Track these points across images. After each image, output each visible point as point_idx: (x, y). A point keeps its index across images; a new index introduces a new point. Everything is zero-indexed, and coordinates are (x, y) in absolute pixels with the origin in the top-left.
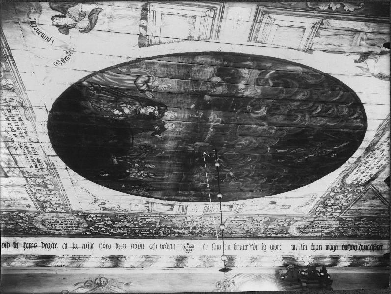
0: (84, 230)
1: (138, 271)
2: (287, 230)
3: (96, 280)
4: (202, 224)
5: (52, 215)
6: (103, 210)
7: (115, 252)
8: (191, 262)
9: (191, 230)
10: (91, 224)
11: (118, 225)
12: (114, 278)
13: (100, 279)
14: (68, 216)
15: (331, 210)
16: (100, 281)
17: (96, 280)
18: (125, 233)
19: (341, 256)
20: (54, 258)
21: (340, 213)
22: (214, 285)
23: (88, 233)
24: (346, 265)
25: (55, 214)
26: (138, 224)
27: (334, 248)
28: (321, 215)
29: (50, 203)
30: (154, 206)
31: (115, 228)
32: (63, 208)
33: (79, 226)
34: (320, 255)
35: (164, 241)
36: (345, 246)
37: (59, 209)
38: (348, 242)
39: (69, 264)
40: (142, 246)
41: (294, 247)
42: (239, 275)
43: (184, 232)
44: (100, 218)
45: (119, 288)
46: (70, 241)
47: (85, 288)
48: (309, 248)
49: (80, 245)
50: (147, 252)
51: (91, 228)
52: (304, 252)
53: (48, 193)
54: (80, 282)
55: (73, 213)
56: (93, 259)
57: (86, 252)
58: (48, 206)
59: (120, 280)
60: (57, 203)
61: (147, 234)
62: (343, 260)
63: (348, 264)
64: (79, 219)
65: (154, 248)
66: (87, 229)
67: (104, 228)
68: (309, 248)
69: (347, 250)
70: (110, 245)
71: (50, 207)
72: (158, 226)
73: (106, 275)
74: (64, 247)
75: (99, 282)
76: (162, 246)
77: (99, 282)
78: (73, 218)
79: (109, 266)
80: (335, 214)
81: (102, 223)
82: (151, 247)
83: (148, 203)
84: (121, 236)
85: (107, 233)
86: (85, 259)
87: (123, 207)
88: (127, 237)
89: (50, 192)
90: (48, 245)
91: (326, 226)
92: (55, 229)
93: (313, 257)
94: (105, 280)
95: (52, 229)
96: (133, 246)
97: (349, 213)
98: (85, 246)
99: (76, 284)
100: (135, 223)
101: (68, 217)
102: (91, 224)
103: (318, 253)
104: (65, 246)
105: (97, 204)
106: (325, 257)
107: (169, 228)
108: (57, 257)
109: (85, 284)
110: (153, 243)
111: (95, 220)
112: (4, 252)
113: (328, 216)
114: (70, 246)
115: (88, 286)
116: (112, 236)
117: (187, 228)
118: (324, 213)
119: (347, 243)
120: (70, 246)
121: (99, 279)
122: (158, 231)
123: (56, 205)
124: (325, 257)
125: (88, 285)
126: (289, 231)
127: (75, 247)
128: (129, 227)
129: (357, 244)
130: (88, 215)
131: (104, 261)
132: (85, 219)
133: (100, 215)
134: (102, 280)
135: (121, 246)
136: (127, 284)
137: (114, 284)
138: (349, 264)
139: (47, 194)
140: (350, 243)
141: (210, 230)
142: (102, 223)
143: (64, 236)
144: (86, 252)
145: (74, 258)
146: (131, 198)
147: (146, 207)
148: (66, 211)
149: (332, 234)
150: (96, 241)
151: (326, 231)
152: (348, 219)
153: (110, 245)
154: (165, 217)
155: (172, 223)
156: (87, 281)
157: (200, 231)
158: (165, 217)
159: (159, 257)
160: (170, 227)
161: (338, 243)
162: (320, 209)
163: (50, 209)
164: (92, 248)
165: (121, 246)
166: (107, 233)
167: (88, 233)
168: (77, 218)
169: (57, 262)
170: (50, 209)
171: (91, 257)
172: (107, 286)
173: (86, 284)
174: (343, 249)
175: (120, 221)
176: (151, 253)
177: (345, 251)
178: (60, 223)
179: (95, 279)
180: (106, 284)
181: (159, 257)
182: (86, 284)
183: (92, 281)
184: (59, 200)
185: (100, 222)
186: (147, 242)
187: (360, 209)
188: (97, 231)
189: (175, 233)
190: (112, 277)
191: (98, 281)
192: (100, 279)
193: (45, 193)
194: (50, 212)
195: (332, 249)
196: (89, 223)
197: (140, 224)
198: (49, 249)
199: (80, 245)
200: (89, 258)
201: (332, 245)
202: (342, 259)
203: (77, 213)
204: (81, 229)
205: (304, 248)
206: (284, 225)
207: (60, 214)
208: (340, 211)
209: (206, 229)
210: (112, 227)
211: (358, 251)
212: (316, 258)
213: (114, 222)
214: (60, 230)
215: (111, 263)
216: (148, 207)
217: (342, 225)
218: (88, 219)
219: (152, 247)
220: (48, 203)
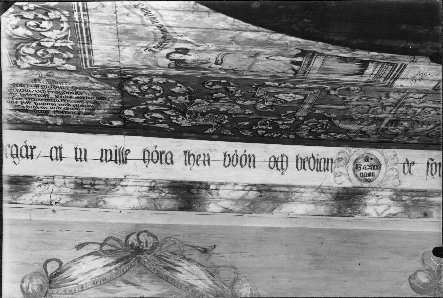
0: (108, 116)
1: (235, 221)
3: (128, 237)
4: (419, 111)
5: (35, 74)
6: (177, 67)
7: (181, 172)
8: (376, 207)
9: (383, 126)
10: (128, 100)
11: (202, 105)
12: (173, 233)
13: (138, 236)
14: (79, 81)
16: (139, 242)
17: (128, 237)
18: (210, 126)
20: (29, 183)
23: (116, 123)
25: (44, 73)
26: (254, 106)
29: (39, 45)
30: (317, 63)
31: (190, 113)
32: (68, 59)
33: (97, 104)
35: (306, 150)
37: (58, 61)
39: (68, 199)
40: (250, 161)
43: (364, 129)
44: (159, 89)
45: (184, 258)
46: (69, 141)
47: (101, 257)
49: (94, 154)
50: (262, 175)
51: (127, 112)
53: (40, 16)
54: (89, 240)
55: (90, 72)
56: (129, 190)
57: (110, 171)
58: (32, 51)
59: (186, 240)
60: (58, 44)
61: (267, 131)
64: (104, 89)
65: (279, 167)
66: (117, 113)
67: (161, 112)
70: (169, 156)
71: (35, 55)
72: (301, 114)
73: (152, 226)
75: (136, 243)
76: (302, 163)
77: (136, 243)
78: (87, 85)
79: (169, 207)
81: (160, 100)
82: (272, 164)
83: (303, 53)
84: (198, 133)
85: (166, 125)
86: (108, 188)
87: (230, 61)
88: (213, 137)
89: (46, 15)
90: (14, 149)
92: (35, 112)
94: (151, 240)
95: (26, 111)
96: (230, 160)
98: (105, 156)
99: (80, 246)
100: (248, 103)
101: (77, 82)
102: (128, 100)
104: (57, 154)
105: (165, 52)
107: (330, 119)
108: (38, 180)
109: (102, 245)
110: (277, 155)
111: (143, 93)
112: (10, 168)
114: (68, 152)
115: (111, 251)
116: (178, 133)
117: (376, 121)
120: (68, 152)
121: (134, 237)
122: (297, 126)
123: (51, 51)
125: (110, 248)
127: (81, 156)
128: (226, 113)
130: (130, 79)
131: (155, 195)
132: (120, 88)
133: (161, 81)
134: (142, 238)
135: (196, 159)
136: (205, 251)
137: (174, 249)
139: (36, 18)
141: (432, 126)
142: (160, 100)
143: (55, 128)
144: (110, 171)
145: (80, 184)
146: (264, 38)
147: (293, 62)
148: (73, 67)
150: (136, 144)
153: (169, 156)
154: (333, 93)
155: (343, 107)
156: (106, 240)
157: (406, 129)
158: (333, 93)
159: (294, 189)
160: (334, 115)
163: (33, 61)
164: (125, 161)
165: (196, 160)
166: (166, 125)
167: (116, 123)
168: (98, 86)
169: (40, 194)
170: (33, 61)
171: (123, 183)
172: (157, 252)
173: (105, 248)
175: (208, 96)
176: (274, 178)
178: (52, 96)
179: (125, 236)
180: (153, 248)
181: (294, 189)
182: (105, 248)
183: (118, 240)
184: (65, 37)
185: (156, 98)
186: (262, 151)
188: (142, 120)
189: (339, 130)
190: (167, 232)
191: (132, 240)
192: (138, 236)
193: (31, 16)
194: (33, 67)
196: (126, 99)
197: (260, 106)
198: (16, 160)
199: (94, 154)
200: (118, 187)
203: (104, 71)
204: (100, 114)
207: (57, 74)
209: (423, 123)
210: (182, 110)
213: (191, 98)
214: (46, 113)
215: (174, 202)
216: (299, 63)
218: (127, 89)
219: (276, 164)
220: (34, 44)
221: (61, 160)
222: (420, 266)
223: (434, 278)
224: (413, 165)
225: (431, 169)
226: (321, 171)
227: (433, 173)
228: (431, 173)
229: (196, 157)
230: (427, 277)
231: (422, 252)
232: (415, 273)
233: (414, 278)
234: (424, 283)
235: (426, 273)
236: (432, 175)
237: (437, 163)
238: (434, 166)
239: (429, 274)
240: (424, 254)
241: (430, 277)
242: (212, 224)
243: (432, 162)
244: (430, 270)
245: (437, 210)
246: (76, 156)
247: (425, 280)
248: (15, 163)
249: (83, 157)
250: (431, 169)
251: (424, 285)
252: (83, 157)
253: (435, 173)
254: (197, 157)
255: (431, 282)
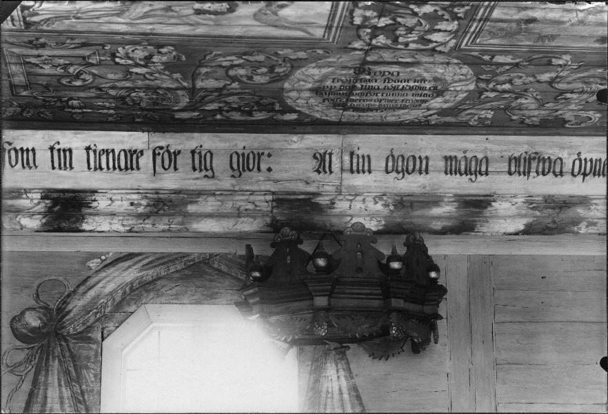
2: (279, 95)
15: (415, 21)
19: (503, 197)
21: (455, 34)
22: (26, 291)
24: (511, 229)
27: (476, 167)
28: (382, 40)
34: (418, 191)
36: (517, 160)
38: (530, 144)
41: (322, 162)
42: (130, 256)
48: (378, 164)
52: (359, 181)
62: (501, 213)
63: (520, 225)
68: (378, 164)
69: (527, 173)
74: (56, 165)
80: (436, 37)
91: (428, 85)
93: (520, 200)
97: (493, 35)
103: (412, 184)
106: (435, 201)
113: (412, 46)
118: (390, 31)
119: (526, 148)
124: (435, 201)
126: (289, 102)
127: (63, 158)
129: (564, 155)
138: (522, 228)
140: (538, 149)
149: (463, 117)
151: (437, 103)
152: (499, 59)
161: (495, 147)
162: (366, 18)
174: (510, 173)
177: (516, 177)
187: (533, 20)
195: (468, 172)
198: (473, 177)
201: (469, 155)
202: (500, 207)
205: (361, 165)
206: (257, 79)
208: (453, 26)
211: (568, 177)
212: (403, 202)
217: (488, 81)
221: (427, 173)
222: (32, 303)
223: (50, 320)
224: (142, 155)
225: (10, 158)
226: (364, 172)
227: (13, 164)
228: (10, 163)
229: (396, 158)
230: (40, 319)
231: (37, 282)
232: (23, 313)
233: (20, 320)
234: (35, 328)
235: (39, 312)
236: (12, 167)
237: (18, 148)
238: (13, 153)
239: (45, 315)
240: (40, 285)
241: (44, 318)
242: (554, 253)
243: (10, 147)
244: (46, 308)
245: (11, 219)
246: (446, 169)
247: (35, 323)
248: (471, 179)
249: (366, 168)
250: (10, 158)
251: (33, 330)
252: (366, 168)
253: (16, 164)
254: (100, 152)
255: (45, 325)
